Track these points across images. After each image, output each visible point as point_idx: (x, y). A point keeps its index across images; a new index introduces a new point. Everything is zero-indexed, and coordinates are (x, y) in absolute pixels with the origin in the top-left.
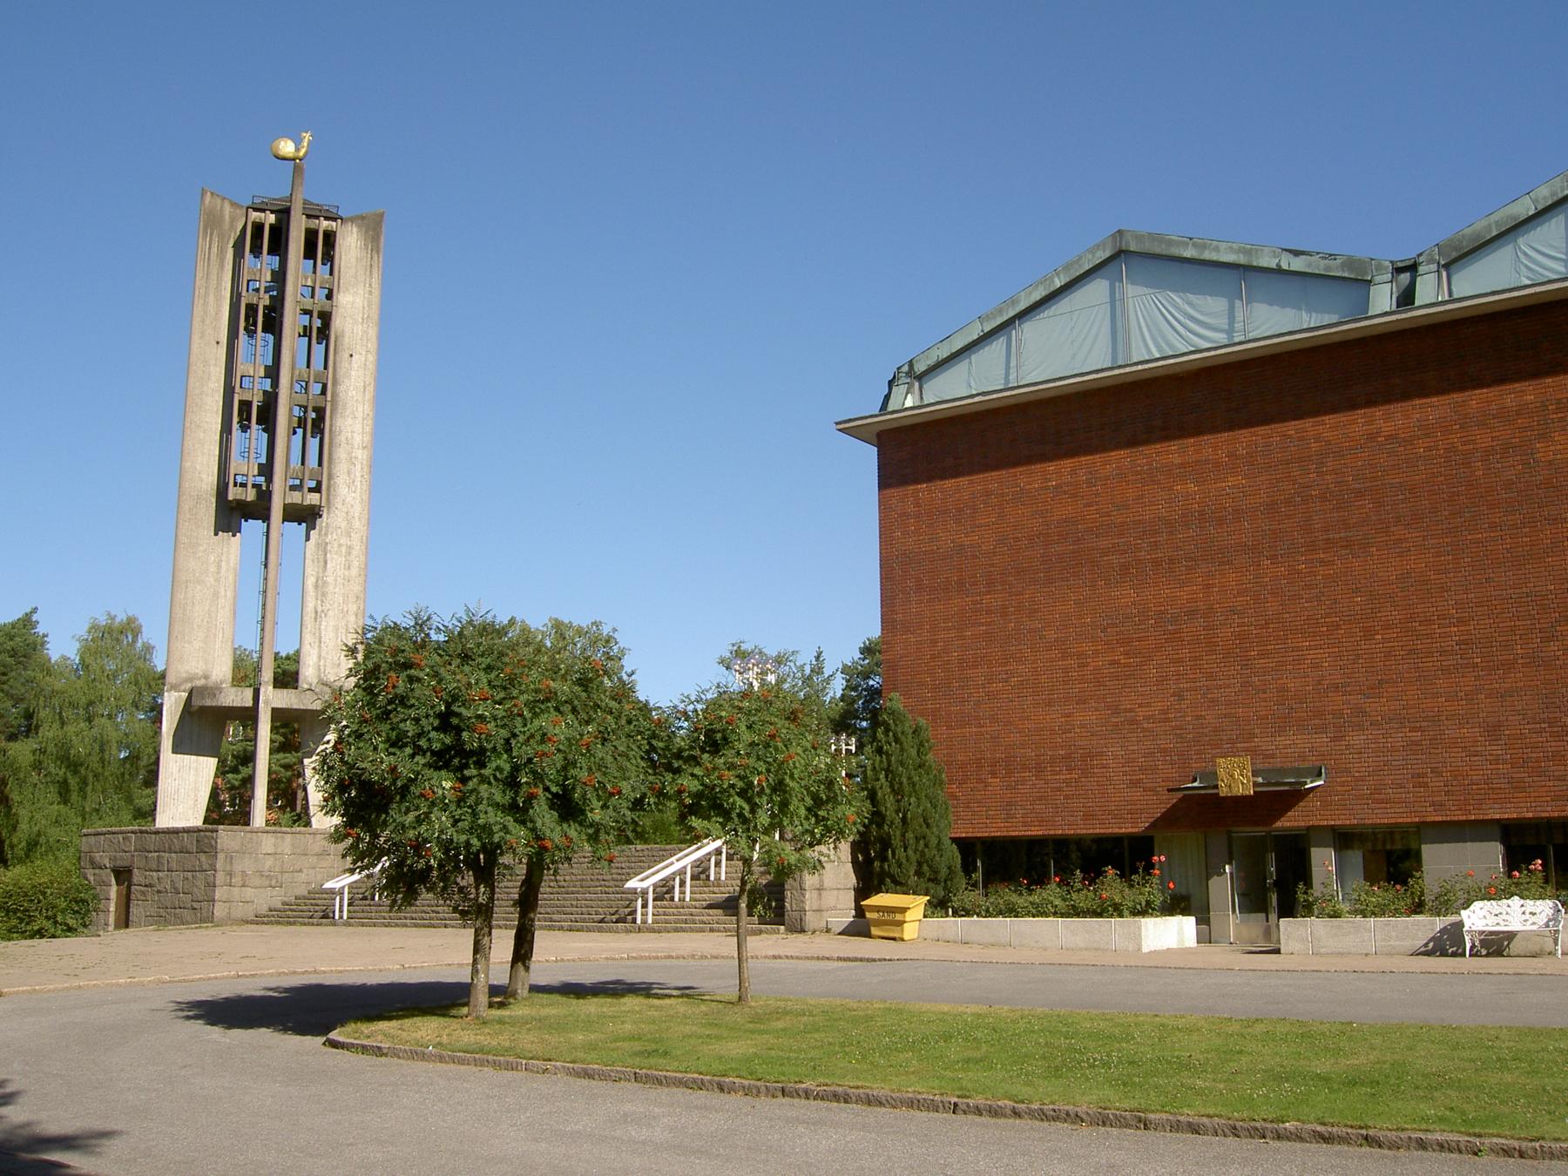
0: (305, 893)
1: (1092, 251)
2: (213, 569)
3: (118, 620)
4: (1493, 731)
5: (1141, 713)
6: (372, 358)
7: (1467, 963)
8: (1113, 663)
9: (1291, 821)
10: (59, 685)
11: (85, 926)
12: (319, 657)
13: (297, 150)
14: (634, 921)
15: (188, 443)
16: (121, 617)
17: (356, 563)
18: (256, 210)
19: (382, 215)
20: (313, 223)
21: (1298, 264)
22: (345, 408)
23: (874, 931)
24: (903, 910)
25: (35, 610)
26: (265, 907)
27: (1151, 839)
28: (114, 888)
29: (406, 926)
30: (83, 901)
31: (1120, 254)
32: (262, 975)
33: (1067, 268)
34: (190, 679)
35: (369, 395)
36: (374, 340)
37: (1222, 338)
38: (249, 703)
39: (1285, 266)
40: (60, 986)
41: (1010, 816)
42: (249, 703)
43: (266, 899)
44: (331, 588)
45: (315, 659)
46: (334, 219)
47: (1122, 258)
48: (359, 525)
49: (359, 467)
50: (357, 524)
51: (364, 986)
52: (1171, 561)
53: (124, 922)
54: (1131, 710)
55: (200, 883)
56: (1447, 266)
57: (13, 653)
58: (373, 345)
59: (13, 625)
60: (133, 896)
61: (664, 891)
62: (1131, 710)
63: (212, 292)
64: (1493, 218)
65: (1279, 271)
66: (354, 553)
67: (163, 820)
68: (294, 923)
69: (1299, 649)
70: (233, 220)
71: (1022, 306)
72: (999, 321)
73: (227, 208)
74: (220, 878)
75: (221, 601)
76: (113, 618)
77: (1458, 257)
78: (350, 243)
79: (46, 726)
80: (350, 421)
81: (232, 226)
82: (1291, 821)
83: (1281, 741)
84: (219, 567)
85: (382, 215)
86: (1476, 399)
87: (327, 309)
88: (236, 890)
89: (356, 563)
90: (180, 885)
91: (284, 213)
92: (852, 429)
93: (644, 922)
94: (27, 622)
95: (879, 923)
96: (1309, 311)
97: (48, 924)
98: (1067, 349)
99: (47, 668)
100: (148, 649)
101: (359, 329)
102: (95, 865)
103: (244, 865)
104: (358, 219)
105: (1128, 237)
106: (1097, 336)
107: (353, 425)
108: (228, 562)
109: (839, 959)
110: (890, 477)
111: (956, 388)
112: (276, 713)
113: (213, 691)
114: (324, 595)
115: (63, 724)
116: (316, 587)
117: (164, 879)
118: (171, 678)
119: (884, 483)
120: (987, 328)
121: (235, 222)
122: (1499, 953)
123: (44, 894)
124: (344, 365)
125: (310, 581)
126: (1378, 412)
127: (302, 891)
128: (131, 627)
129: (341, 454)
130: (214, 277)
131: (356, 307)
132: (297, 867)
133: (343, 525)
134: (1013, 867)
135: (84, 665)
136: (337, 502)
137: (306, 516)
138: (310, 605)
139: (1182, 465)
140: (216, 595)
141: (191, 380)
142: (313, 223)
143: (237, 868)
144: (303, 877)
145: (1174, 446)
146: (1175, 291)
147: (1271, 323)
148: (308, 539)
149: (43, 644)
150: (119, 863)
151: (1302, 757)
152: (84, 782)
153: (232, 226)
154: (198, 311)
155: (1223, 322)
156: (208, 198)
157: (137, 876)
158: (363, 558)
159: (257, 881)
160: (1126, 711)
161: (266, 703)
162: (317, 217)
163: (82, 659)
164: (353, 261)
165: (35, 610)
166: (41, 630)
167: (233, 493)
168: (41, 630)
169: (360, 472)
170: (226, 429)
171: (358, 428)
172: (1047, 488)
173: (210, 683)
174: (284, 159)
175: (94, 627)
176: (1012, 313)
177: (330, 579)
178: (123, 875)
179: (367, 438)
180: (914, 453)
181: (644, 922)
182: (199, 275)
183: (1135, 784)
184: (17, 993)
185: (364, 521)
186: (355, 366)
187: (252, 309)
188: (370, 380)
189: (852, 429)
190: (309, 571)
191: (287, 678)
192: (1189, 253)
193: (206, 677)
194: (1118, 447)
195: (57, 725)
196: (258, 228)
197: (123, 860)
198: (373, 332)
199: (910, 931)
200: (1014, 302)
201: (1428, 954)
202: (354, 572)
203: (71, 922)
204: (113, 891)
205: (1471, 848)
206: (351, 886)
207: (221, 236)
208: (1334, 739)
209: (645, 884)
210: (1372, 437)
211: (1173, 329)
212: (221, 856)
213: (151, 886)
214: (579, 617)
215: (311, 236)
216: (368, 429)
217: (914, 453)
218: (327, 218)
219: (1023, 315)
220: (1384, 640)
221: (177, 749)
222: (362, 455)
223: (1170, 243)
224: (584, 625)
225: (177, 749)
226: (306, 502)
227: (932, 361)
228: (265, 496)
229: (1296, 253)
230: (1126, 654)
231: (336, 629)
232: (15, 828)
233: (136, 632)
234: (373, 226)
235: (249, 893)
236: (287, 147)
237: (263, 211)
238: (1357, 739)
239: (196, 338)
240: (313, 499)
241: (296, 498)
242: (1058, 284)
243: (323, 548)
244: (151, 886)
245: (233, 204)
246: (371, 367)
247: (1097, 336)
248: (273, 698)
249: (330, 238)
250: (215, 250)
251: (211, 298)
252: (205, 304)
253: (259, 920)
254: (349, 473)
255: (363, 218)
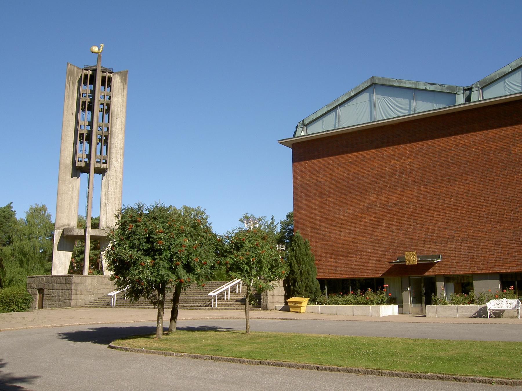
0: (102, 297)
1: (363, 83)
2: (71, 189)
3: (39, 206)
4: (497, 243)
5: (380, 237)
6: (124, 119)
7: (488, 320)
8: (370, 220)
9: (430, 273)
10: (20, 228)
11: (28, 308)
12: (106, 218)
13: (99, 50)
14: (211, 306)
15: (63, 147)
16: (40, 205)
17: (118, 187)
18: (85, 70)
19: (127, 71)
20: (104, 74)
21: (432, 88)
22: (115, 136)
23: (291, 310)
24: (301, 303)
25: (12, 203)
26: (88, 302)
27: (383, 279)
28: (38, 295)
29: (135, 308)
30: (28, 300)
31: (373, 85)
32: (87, 324)
33: (355, 89)
34: (63, 226)
35: (123, 131)
36: (125, 113)
37: (407, 112)
38: (83, 234)
39: (428, 89)
40: (20, 328)
41: (336, 271)
42: (83, 234)
43: (88, 299)
44: (110, 195)
45: (105, 219)
46: (111, 73)
47: (374, 86)
48: (120, 175)
49: (119, 155)
50: (119, 174)
51: (121, 328)
52: (390, 186)
53: (41, 306)
54: (377, 236)
55: (67, 294)
56: (482, 89)
57: (4, 217)
58: (124, 115)
59: (4, 208)
60: (44, 298)
61: (221, 296)
62: (377, 236)
63: (70, 97)
64: (497, 72)
65: (426, 90)
66: (118, 184)
67: (54, 273)
68: (98, 307)
69: (432, 216)
70: (78, 73)
71: (340, 102)
72: (333, 107)
73: (76, 69)
74: (73, 292)
75: (74, 200)
76: (38, 206)
77: (485, 85)
78: (117, 81)
79: (15, 241)
80: (116, 140)
81: (77, 75)
82: (430, 273)
83: (427, 246)
84: (73, 188)
85: (127, 71)
86: (491, 133)
87: (109, 103)
88: (79, 296)
89: (118, 187)
90: (60, 294)
91: (95, 71)
92: (284, 143)
93: (214, 306)
94: (9, 207)
95: (293, 307)
96: (436, 103)
97: (16, 307)
98: (355, 116)
99: (16, 222)
100: (49, 216)
101: (119, 109)
102: (31, 288)
103: (81, 287)
104: (119, 73)
105: (375, 79)
106: (365, 112)
107: (118, 141)
108: (76, 187)
109: (279, 319)
110: (296, 159)
111: (318, 129)
112: (92, 237)
113: (71, 230)
114: (108, 198)
115: (21, 241)
116: (105, 195)
117: (55, 292)
118: (57, 226)
119: (294, 160)
120: (329, 109)
121: (78, 74)
122: (499, 317)
123: (15, 297)
124: (114, 121)
125: (103, 193)
126: (459, 137)
127: (101, 296)
128: (44, 209)
129: (114, 151)
130: (71, 92)
131: (119, 102)
132: (99, 288)
133: (114, 174)
134: (337, 288)
135: (28, 221)
136: (112, 167)
137: (102, 172)
138: (103, 201)
139: (393, 155)
140: (72, 198)
141: (64, 126)
142: (104, 74)
143: (79, 288)
144: (101, 292)
145: (391, 148)
146: (391, 97)
147: (423, 107)
148: (102, 179)
149: (14, 214)
150: (40, 287)
151: (433, 252)
152: (28, 260)
153: (77, 75)
154: (66, 103)
155: (407, 107)
156: (69, 66)
157: (46, 291)
158: (121, 186)
159: (85, 293)
160: (375, 236)
161: (89, 234)
162: (106, 72)
163: (27, 219)
164: (118, 87)
165: (12, 203)
166: (14, 209)
167: (78, 164)
168: (14, 209)
169: (120, 157)
170: (75, 143)
171: (119, 142)
172: (349, 162)
173: (70, 227)
174: (95, 53)
175: (31, 209)
176: (337, 104)
177: (110, 193)
178: (41, 291)
179: (122, 146)
180: (304, 150)
181: (214, 306)
182: (66, 91)
183: (378, 261)
184: (6, 330)
185: (121, 173)
186: (118, 122)
187: (84, 103)
188: (123, 126)
189: (284, 143)
190: (103, 190)
191: (95, 225)
192: (396, 84)
193: (69, 225)
194: (372, 149)
195: (19, 241)
196: (86, 76)
197: (41, 286)
198: (124, 111)
199: (303, 310)
200: (337, 100)
201: (475, 317)
202: (118, 190)
203: (24, 307)
204: (38, 296)
205: (490, 282)
206: (117, 295)
207: (74, 79)
208: (444, 246)
209: (215, 294)
210: (457, 145)
211: (391, 109)
212: (74, 285)
213: (50, 294)
214: (193, 205)
215: (104, 78)
216: (122, 143)
217: (304, 150)
218: (109, 73)
219: (340, 105)
220: (461, 213)
221: (59, 249)
222: (120, 151)
223: (390, 81)
224: (194, 208)
225: (59, 249)
226: (102, 167)
227: (310, 120)
228: (88, 165)
229: (432, 84)
230: (375, 217)
231: (112, 209)
232: (5, 275)
233: (45, 210)
234: (124, 75)
235: (83, 297)
236: (96, 49)
237: (88, 70)
238: (452, 246)
239: (65, 112)
240: (104, 166)
241: (98, 165)
242: (352, 94)
243: (108, 182)
244: (50, 294)
245: (78, 68)
246: (124, 122)
247: (365, 112)
248: (91, 232)
249: (110, 79)
250: (71, 83)
251: (70, 99)
252: (68, 101)
253: (86, 306)
254: (116, 157)
255: (121, 72)
